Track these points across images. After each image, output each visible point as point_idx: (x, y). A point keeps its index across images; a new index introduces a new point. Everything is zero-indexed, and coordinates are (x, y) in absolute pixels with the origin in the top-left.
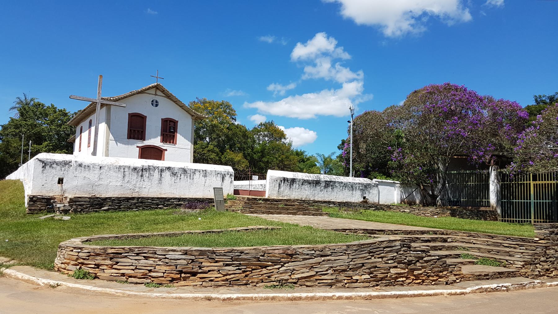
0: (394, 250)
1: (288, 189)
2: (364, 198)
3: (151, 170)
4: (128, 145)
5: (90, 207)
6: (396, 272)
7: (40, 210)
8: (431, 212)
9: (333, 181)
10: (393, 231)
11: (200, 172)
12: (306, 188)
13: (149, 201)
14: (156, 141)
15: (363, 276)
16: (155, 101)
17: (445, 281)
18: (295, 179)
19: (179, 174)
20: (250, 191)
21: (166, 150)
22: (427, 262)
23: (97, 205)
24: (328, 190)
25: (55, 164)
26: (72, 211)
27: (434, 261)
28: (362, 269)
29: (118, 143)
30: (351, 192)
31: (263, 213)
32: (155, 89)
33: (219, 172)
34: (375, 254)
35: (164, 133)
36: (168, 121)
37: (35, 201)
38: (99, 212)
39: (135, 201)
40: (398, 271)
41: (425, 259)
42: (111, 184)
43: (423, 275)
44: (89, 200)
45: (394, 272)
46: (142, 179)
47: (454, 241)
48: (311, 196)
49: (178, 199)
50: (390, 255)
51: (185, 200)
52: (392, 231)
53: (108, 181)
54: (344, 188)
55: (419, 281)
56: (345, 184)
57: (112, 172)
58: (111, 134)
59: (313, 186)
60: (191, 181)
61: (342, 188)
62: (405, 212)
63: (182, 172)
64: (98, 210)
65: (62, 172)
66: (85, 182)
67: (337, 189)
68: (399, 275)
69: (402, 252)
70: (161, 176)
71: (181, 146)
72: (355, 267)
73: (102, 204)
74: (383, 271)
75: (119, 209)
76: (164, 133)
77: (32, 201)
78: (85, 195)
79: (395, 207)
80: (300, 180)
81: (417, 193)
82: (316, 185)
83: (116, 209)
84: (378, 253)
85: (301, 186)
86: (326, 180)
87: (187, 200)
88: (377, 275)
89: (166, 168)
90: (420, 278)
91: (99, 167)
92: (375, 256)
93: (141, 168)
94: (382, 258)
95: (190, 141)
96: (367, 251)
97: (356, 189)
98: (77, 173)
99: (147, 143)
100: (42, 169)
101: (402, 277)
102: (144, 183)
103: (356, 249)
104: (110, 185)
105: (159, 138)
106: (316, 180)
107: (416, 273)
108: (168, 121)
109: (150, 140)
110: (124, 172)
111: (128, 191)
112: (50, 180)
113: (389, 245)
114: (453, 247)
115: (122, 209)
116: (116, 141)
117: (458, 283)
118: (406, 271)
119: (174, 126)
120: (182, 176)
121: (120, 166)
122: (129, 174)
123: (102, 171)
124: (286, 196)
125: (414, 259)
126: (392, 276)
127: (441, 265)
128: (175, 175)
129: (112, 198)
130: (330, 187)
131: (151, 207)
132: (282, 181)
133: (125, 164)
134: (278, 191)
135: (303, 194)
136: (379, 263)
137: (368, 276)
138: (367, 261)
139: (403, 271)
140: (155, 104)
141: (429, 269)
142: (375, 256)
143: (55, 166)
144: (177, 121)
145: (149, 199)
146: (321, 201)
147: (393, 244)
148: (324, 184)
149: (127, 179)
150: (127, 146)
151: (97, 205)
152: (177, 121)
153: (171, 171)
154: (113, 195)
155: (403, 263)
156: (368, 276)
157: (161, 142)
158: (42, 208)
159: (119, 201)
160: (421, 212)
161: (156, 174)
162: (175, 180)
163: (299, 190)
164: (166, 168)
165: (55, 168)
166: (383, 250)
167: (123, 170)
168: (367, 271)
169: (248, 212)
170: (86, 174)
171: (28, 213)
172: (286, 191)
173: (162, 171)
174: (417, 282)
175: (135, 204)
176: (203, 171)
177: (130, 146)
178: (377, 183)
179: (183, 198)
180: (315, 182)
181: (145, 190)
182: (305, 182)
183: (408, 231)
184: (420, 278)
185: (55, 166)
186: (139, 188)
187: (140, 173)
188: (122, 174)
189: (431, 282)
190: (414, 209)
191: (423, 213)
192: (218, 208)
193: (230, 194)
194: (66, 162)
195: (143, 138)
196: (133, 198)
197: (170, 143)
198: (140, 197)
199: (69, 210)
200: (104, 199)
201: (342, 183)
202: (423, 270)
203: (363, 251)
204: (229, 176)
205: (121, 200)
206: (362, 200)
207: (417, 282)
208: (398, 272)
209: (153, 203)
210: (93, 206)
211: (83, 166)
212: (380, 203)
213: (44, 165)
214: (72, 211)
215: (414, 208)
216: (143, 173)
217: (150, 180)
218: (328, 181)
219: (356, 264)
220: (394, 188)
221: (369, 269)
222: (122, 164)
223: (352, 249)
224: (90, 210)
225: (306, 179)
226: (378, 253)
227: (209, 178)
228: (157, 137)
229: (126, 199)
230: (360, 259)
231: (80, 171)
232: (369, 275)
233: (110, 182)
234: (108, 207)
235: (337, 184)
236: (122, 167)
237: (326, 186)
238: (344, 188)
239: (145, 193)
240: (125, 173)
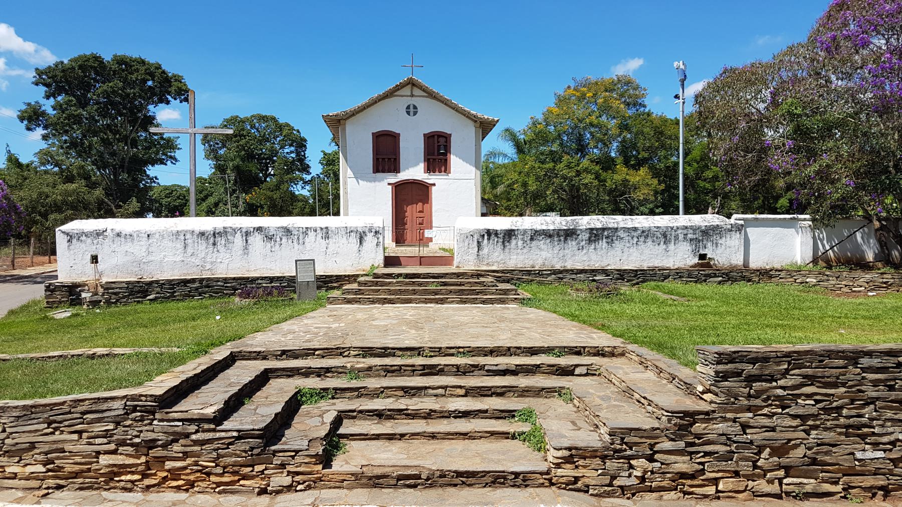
0: (107, 417)
1: (499, 249)
2: (703, 257)
3: (228, 235)
4: (374, 182)
5: (129, 295)
6: (111, 462)
7: (60, 302)
8: (867, 283)
9: (610, 229)
10: (443, 350)
11: (316, 231)
12: (542, 246)
13: (219, 283)
14: (415, 172)
15: (28, 466)
16: (411, 107)
17: (258, 485)
18: (513, 230)
19: (278, 237)
20: (421, 257)
21: (434, 185)
22: (196, 443)
23: (138, 292)
24: (597, 246)
25: (84, 236)
26: (104, 302)
27: (223, 441)
28: (32, 453)
29: (359, 180)
30: (663, 246)
31: (372, 301)
32: (410, 86)
33: (352, 229)
34: (62, 425)
35: (429, 157)
36: (436, 137)
37: (52, 291)
38: (142, 303)
39: (197, 285)
40: (118, 460)
41: (194, 437)
42: (166, 259)
43: (188, 471)
44: (126, 286)
45: (105, 462)
46: (215, 249)
47: (597, 373)
48: (556, 260)
49: (270, 279)
50: (99, 428)
51: (282, 280)
52: (440, 348)
53: (161, 256)
54: (642, 239)
55: (181, 482)
56: (643, 232)
57: (165, 242)
58: (348, 168)
59: (560, 240)
60: (301, 247)
61: (636, 240)
62: (807, 282)
63: (284, 233)
64: (140, 299)
65: (95, 247)
66: (128, 258)
67: (623, 244)
68: (122, 469)
69: (128, 422)
70: (247, 242)
71: (457, 176)
72: (13, 449)
73: (147, 291)
74: (78, 459)
75: (172, 297)
76: (429, 157)
77: (49, 291)
78: (130, 278)
79: (783, 274)
80: (525, 231)
81: (869, 237)
82: (566, 239)
83: (168, 298)
84: (66, 423)
85: (528, 242)
86: (592, 226)
87: (286, 280)
88: (63, 468)
89: (254, 228)
90: (183, 477)
91: (147, 236)
92: (61, 429)
93: (212, 233)
94: (80, 433)
95: (474, 165)
96: (41, 420)
97: (677, 238)
98: (115, 246)
99: (406, 174)
100: (67, 244)
101: (133, 473)
102: (219, 254)
103: (17, 414)
104: (165, 261)
105: (422, 166)
106: (565, 228)
107: (169, 465)
108: (436, 137)
109: (407, 171)
110: (185, 240)
111: (195, 269)
112: (80, 259)
113: (94, 407)
114: (544, 389)
115: (178, 298)
116: (356, 178)
117: (300, 493)
118: (139, 462)
119: (445, 144)
120: (284, 240)
121: (178, 232)
122: (194, 242)
123: (151, 241)
124: (496, 264)
125: (160, 438)
126: (100, 469)
127: (245, 452)
128: (271, 238)
129: (161, 282)
130: (604, 240)
131: (224, 293)
132: (484, 235)
133: (186, 228)
134: (478, 255)
135: (535, 257)
136: (72, 442)
137: (41, 469)
138: (41, 439)
139: (131, 461)
140: (412, 110)
141: (207, 459)
142: (61, 429)
143: (84, 238)
144: (450, 135)
145: (219, 281)
146: (572, 270)
147: (104, 406)
148: (588, 235)
149: (190, 250)
150: (373, 184)
151: (138, 292)
152: (450, 135)
153: (263, 233)
154: (171, 276)
155: (132, 445)
156: (41, 469)
157: (425, 173)
158: (63, 300)
159: (171, 285)
160: (843, 283)
161: (238, 240)
162: (271, 247)
163: (525, 251)
164: (254, 228)
165: (85, 242)
166: (82, 418)
167: (183, 238)
168: (41, 458)
169: (340, 301)
170: (128, 246)
171: (45, 308)
172: (496, 254)
173: (247, 234)
174: (175, 483)
175: (197, 289)
176: (322, 229)
177: (377, 183)
178: (742, 222)
179: (278, 277)
180: (562, 233)
181: (222, 266)
182: (536, 235)
183: (486, 349)
184: (183, 477)
185: (84, 238)
186: (212, 263)
187: (211, 241)
188: (183, 243)
189: (214, 486)
190: (827, 275)
191: (846, 286)
192: (302, 295)
193: (376, 265)
194: (98, 231)
195: (396, 169)
196: (193, 281)
197: (440, 172)
198: (204, 278)
199: (100, 301)
200: (148, 284)
201: (635, 229)
202: (189, 461)
203: (34, 419)
204: (372, 234)
205: (174, 284)
206: (696, 260)
207: (175, 483)
208: (117, 462)
209: (226, 287)
210: (134, 295)
211: (123, 235)
212: (754, 264)
213: (69, 238)
214: (104, 302)
215: (828, 273)
216: (216, 240)
217: (228, 249)
218: (597, 229)
219: (17, 444)
220: (793, 230)
221: (46, 453)
222: (180, 229)
223: (9, 415)
224: (130, 301)
225: (539, 228)
226: (66, 423)
227: (334, 240)
228: (418, 164)
229: (182, 282)
230: (28, 434)
231: (119, 243)
232: (45, 465)
233: (165, 256)
234: (155, 295)
235: (621, 234)
236: (181, 232)
237: (593, 238)
238: (642, 239)
239: (222, 272)
240: (186, 241)
